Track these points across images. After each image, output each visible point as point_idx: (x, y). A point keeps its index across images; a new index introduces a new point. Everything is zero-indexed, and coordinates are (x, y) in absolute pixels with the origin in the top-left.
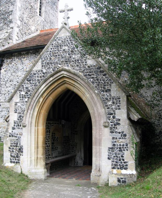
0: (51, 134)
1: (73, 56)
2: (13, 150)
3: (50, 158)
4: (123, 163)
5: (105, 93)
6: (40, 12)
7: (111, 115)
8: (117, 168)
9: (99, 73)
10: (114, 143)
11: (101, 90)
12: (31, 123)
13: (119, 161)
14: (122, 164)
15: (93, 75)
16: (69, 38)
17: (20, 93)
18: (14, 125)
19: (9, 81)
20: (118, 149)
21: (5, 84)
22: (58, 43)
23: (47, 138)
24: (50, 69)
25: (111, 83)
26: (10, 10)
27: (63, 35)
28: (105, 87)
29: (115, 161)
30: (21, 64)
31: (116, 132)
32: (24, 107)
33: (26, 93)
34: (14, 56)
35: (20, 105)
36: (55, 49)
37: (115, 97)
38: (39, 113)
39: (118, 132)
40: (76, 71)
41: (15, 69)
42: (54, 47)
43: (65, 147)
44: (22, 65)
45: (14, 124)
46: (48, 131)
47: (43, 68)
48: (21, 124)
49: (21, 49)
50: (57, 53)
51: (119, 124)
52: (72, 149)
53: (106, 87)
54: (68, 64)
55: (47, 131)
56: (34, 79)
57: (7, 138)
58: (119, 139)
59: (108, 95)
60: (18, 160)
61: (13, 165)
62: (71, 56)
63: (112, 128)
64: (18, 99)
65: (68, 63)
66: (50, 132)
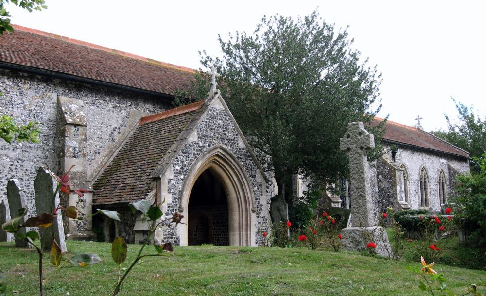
1: (228, 134)
17: (174, 166)
18: (168, 210)
44: (21, 97)
45: (167, 208)
49: (66, 75)
51: (261, 209)
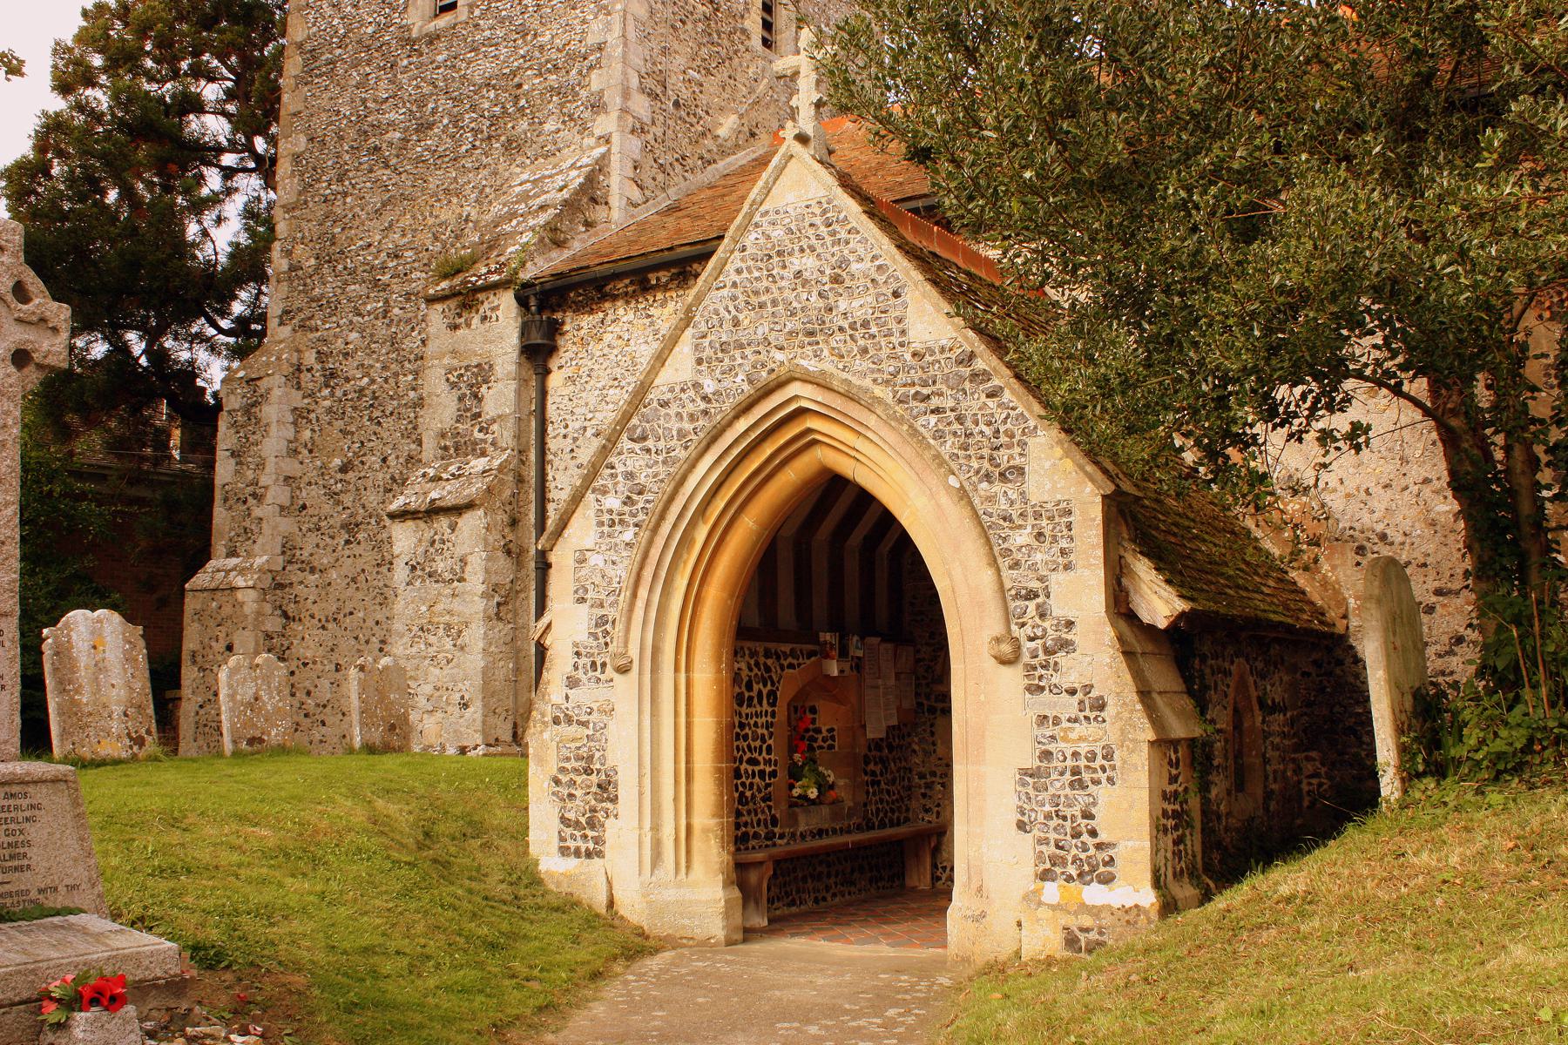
0: (781, 709)
1: (843, 305)
2: (573, 792)
3: (782, 836)
4: (1092, 851)
5: (998, 488)
6: (767, 26)
7: (1030, 599)
8: (1063, 873)
9: (967, 385)
10: (1044, 744)
11: (978, 472)
12: (656, 651)
13: (1073, 837)
14: (1089, 853)
15: (940, 394)
16: (818, 211)
17: (598, 500)
19: (590, 432)
20: (1068, 776)
21: (572, 451)
22: (769, 237)
23: (760, 731)
24: (737, 374)
25: (1024, 433)
26: (591, 40)
27: (791, 197)
28: (995, 453)
29: (1052, 843)
30: (651, 338)
31: (1055, 689)
32: (619, 572)
33: (625, 503)
34: (614, 298)
35: (601, 564)
36: (756, 274)
37: (1049, 506)
38: (693, 600)
39: (1065, 686)
40: (855, 380)
41: (618, 370)
42: (751, 263)
43: (875, 783)
45: (572, 660)
46: (765, 692)
47: (700, 372)
48: (608, 660)
50: (768, 290)
52: (924, 795)
53: (1003, 456)
54: (818, 343)
55: (760, 693)
56: (660, 431)
57: (541, 732)
58: (1070, 725)
59: (1014, 497)
60: (597, 840)
61: (571, 863)
62: (831, 301)
63: (1035, 668)
64: (592, 533)
65: (820, 338)
66: (775, 698)
